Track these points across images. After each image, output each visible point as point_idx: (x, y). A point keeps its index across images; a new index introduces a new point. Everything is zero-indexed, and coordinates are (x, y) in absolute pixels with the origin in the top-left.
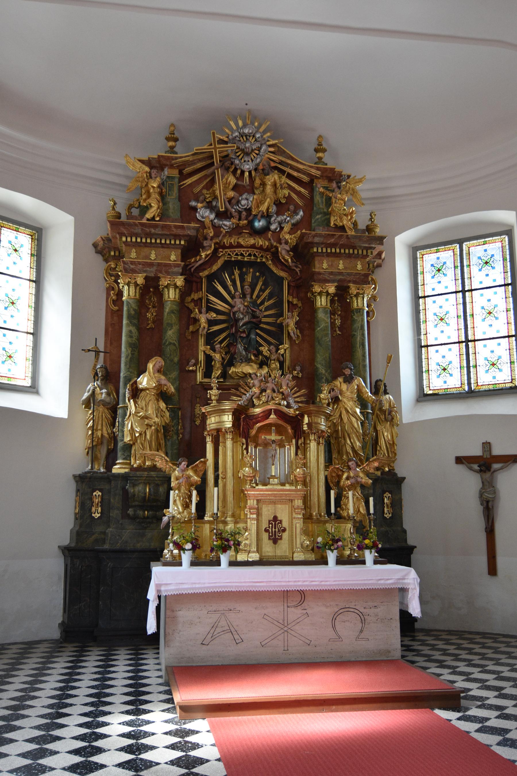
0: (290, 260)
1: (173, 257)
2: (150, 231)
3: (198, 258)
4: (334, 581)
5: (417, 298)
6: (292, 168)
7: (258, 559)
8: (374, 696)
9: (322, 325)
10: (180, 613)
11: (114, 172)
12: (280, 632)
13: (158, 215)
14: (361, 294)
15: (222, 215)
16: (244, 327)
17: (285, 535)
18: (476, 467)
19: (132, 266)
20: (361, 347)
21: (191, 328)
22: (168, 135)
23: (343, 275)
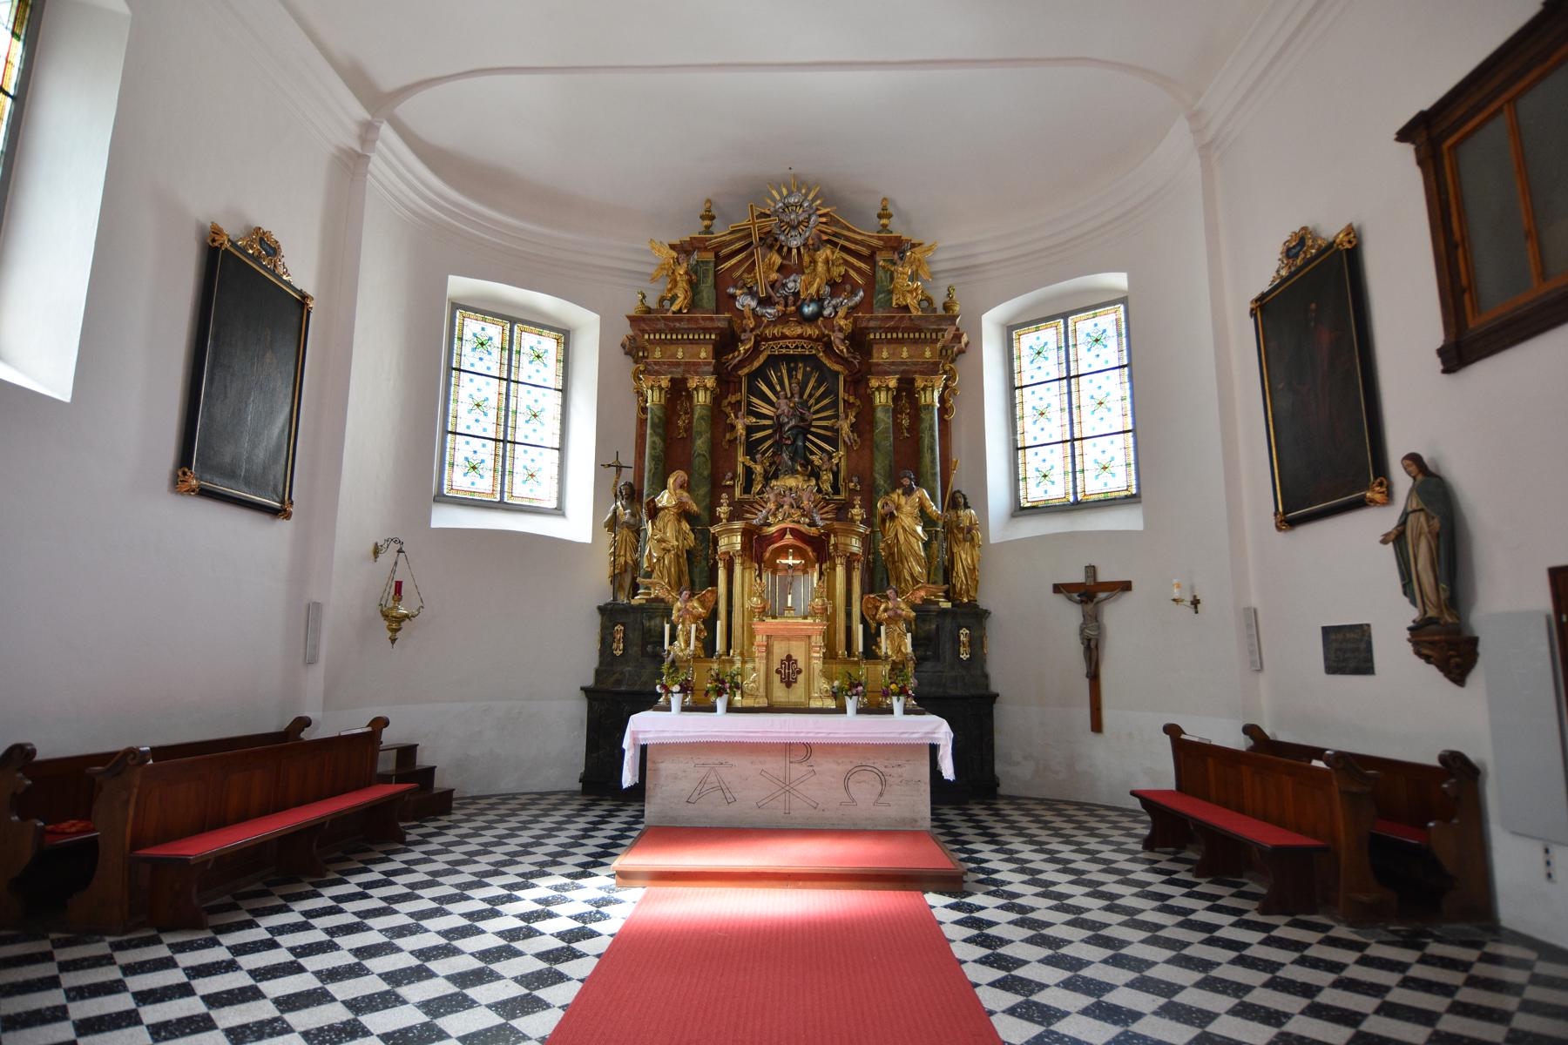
1: (703, 355)
5: (1012, 388)
6: (847, 238)
9: (881, 427)
10: (663, 766)
11: (640, 265)
15: (765, 302)
17: (801, 678)
18: (1075, 596)
21: (728, 436)
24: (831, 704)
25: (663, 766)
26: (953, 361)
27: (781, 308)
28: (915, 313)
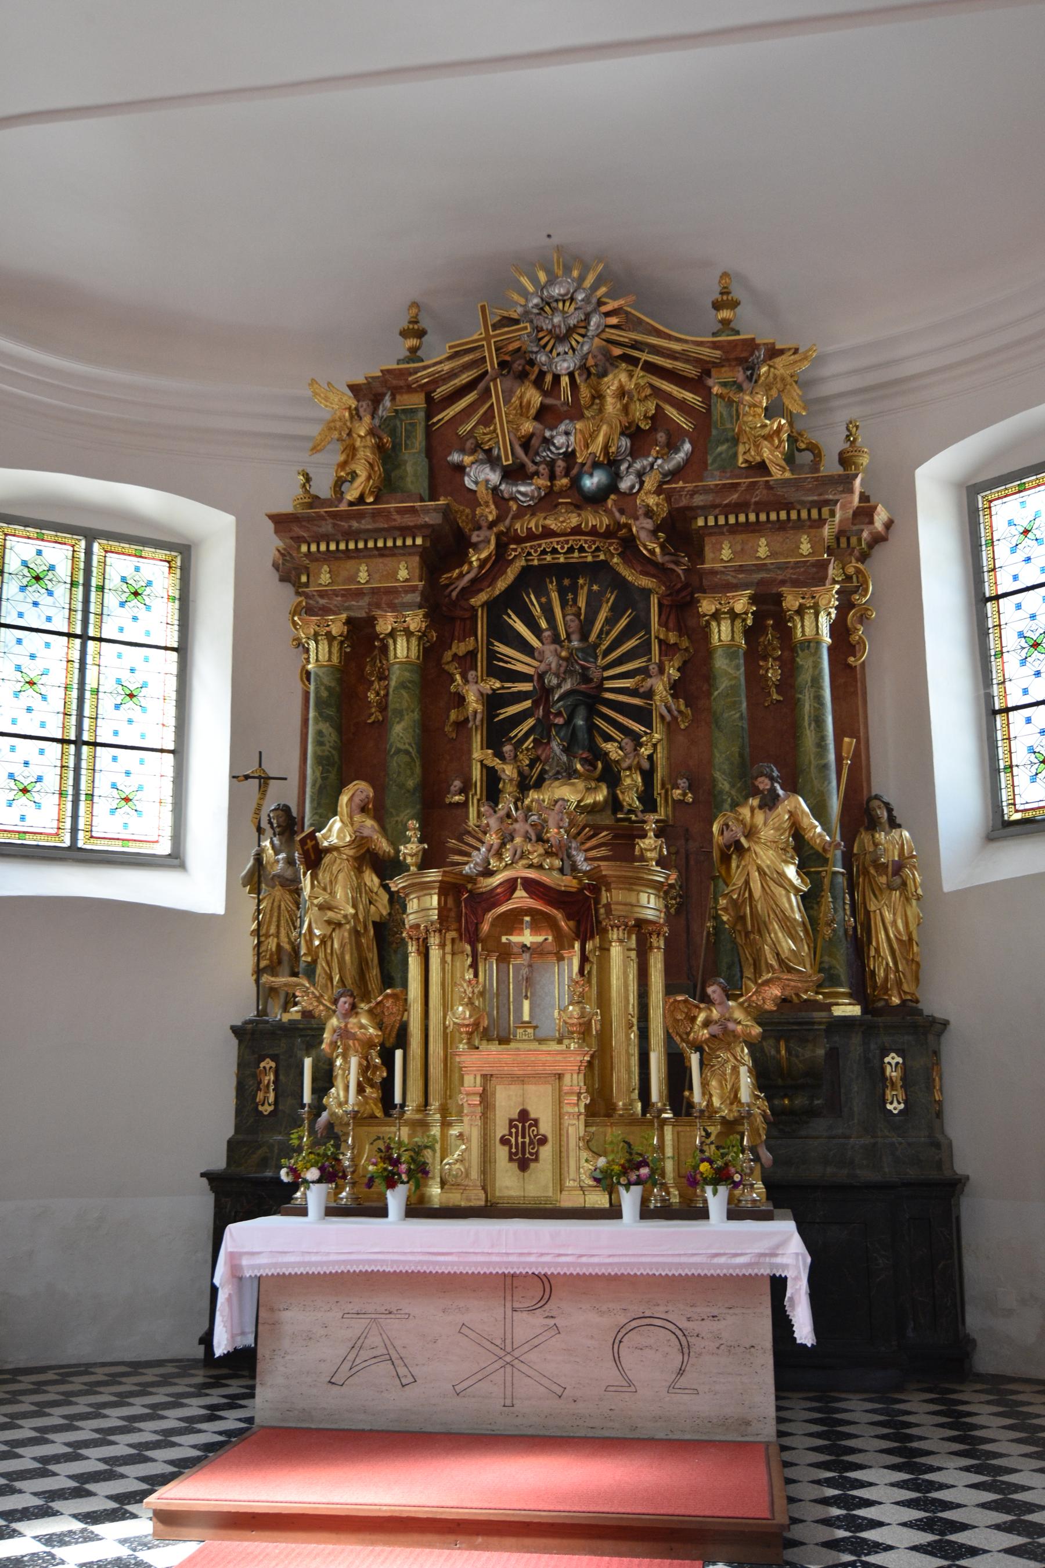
0: (658, 550)
1: (403, 574)
2: (350, 527)
3: (465, 568)
4: (610, 1256)
5: (980, 600)
7: (482, 1203)
8: (567, 1521)
9: (723, 684)
10: (286, 1316)
11: (295, 432)
12: (497, 1366)
13: (371, 493)
14: (810, 608)
15: (514, 473)
16: (561, 703)
17: (546, 1152)
19: (322, 601)
20: (813, 725)
21: (453, 715)
22: (404, 324)
23: (768, 570)
24: (599, 1200)
25: (286, 1316)
26: (864, 557)
27: (543, 482)
28: (778, 473)
